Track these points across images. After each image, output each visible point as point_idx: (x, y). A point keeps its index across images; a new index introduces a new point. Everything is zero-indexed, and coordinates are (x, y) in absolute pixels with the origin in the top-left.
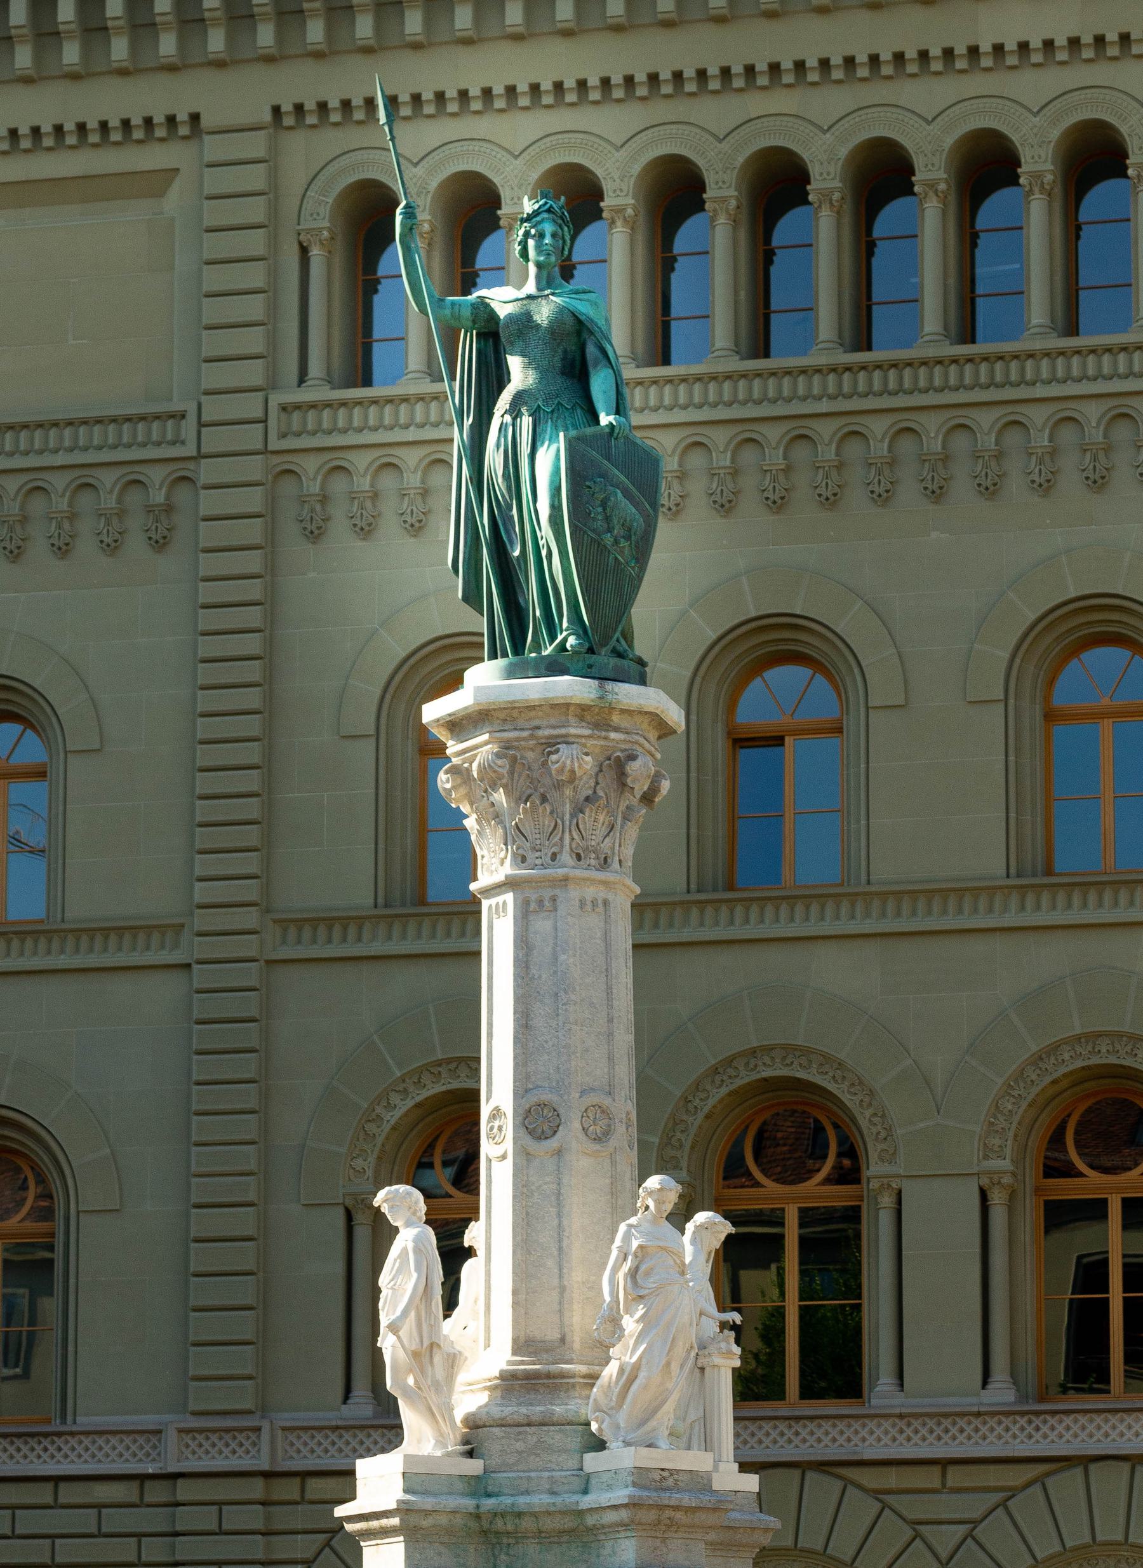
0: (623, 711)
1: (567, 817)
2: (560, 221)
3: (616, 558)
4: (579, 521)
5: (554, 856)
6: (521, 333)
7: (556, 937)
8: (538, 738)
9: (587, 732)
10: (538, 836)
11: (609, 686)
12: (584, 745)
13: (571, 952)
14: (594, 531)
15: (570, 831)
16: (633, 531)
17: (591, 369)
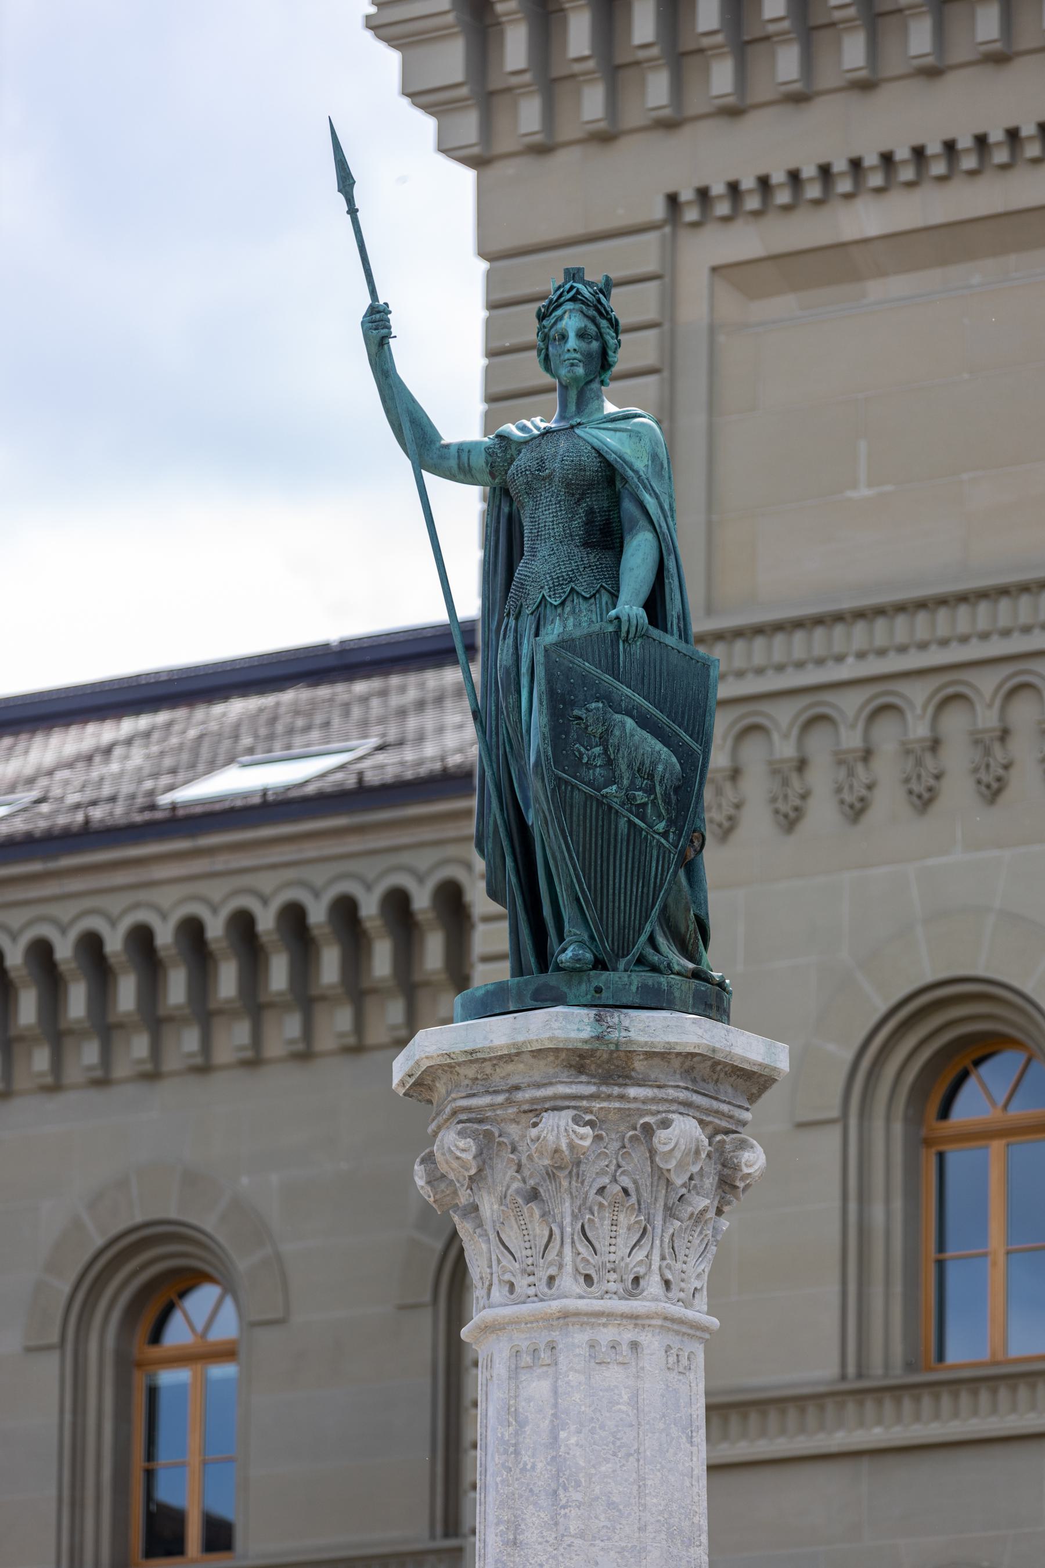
0: (650, 1055)
1: (568, 1220)
2: (592, 312)
3: (629, 821)
4: (564, 771)
5: (551, 1279)
6: (531, 488)
7: (555, 1405)
8: (519, 1103)
9: (592, 1089)
10: (529, 1252)
11: (614, 1017)
12: (588, 1110)
13: (573, 1428)
14: (589, 784)
15: (573, 1242)
16: (657, 779)
17: (625, 534)
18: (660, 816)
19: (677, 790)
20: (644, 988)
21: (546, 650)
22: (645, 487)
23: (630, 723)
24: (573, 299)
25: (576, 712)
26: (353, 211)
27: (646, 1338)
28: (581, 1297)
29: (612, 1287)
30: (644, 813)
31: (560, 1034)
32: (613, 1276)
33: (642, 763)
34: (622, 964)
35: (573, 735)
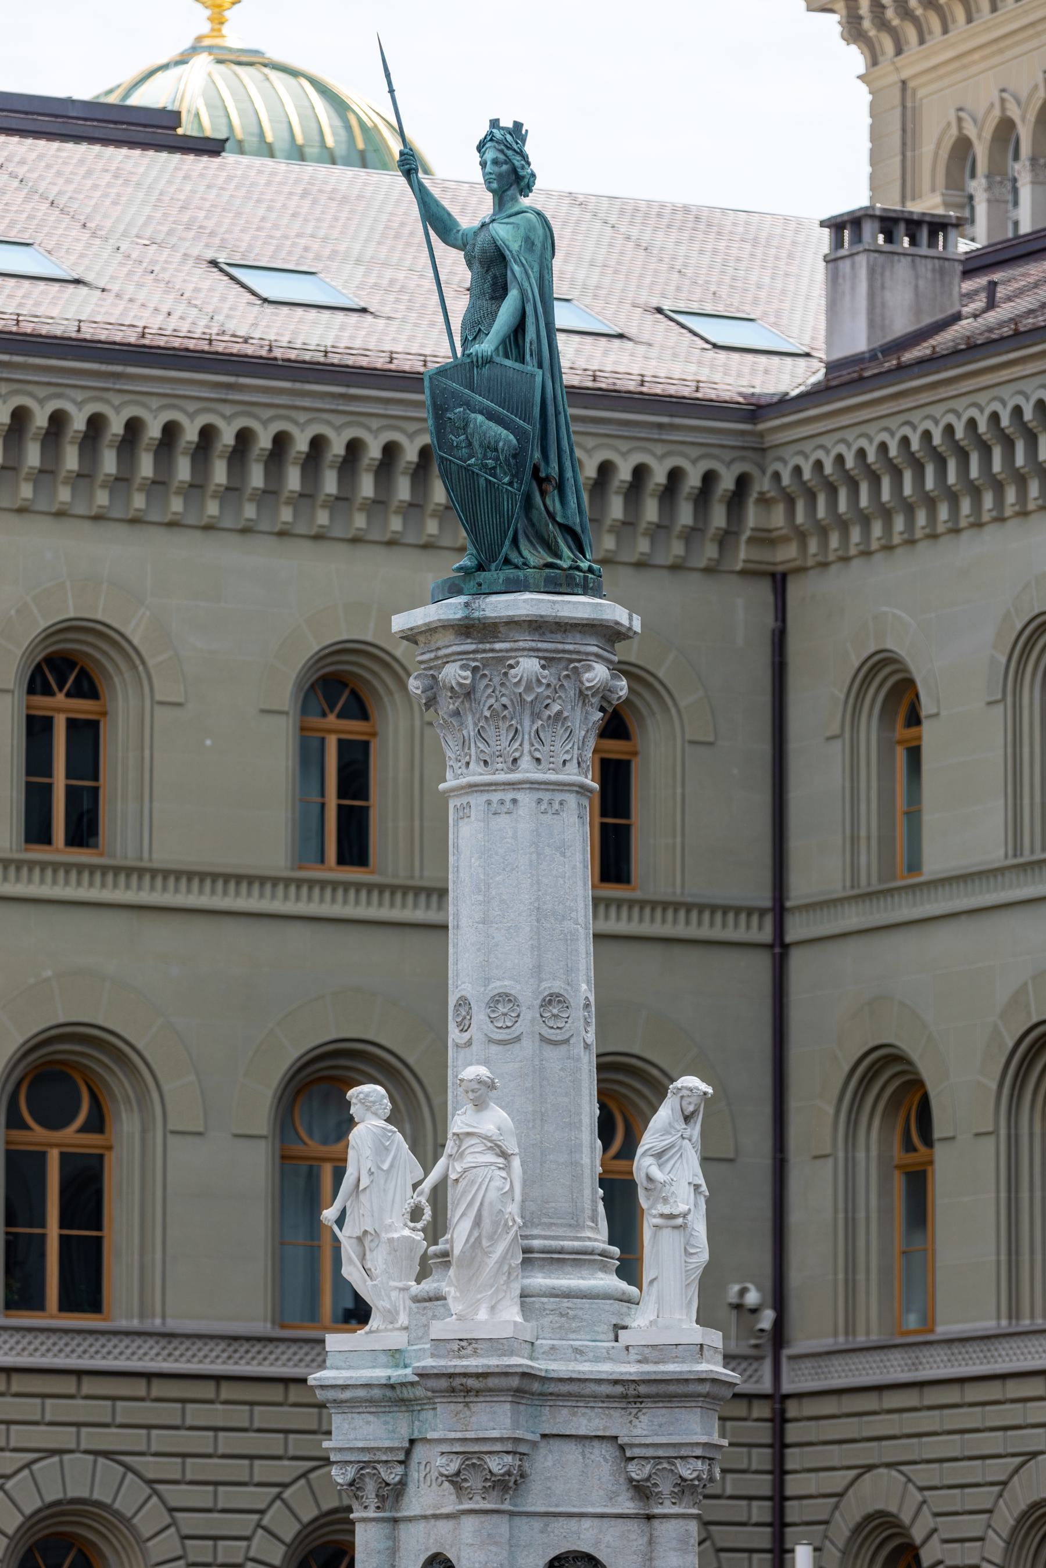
3: (486, 479)
18: (505, 474)
19: (515, 456)
20: (507, 580)
21: (430, 378)
22: (515, 261)
23: (480, 418)
24: (491, 140)
25: (448, 415)
26: (391, 91)
27: (520, 796)
28: (481, 774)
29: (500, 766)
30: (495, 473)
31: (443, 617)
32: (500, 759)
33: (489, 443)
34: (493, 566)
35: (448, 429)
